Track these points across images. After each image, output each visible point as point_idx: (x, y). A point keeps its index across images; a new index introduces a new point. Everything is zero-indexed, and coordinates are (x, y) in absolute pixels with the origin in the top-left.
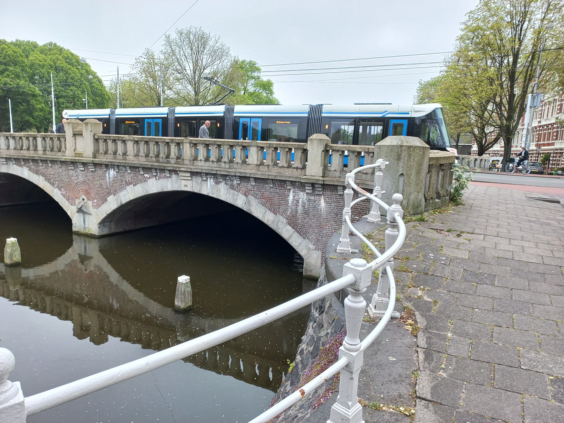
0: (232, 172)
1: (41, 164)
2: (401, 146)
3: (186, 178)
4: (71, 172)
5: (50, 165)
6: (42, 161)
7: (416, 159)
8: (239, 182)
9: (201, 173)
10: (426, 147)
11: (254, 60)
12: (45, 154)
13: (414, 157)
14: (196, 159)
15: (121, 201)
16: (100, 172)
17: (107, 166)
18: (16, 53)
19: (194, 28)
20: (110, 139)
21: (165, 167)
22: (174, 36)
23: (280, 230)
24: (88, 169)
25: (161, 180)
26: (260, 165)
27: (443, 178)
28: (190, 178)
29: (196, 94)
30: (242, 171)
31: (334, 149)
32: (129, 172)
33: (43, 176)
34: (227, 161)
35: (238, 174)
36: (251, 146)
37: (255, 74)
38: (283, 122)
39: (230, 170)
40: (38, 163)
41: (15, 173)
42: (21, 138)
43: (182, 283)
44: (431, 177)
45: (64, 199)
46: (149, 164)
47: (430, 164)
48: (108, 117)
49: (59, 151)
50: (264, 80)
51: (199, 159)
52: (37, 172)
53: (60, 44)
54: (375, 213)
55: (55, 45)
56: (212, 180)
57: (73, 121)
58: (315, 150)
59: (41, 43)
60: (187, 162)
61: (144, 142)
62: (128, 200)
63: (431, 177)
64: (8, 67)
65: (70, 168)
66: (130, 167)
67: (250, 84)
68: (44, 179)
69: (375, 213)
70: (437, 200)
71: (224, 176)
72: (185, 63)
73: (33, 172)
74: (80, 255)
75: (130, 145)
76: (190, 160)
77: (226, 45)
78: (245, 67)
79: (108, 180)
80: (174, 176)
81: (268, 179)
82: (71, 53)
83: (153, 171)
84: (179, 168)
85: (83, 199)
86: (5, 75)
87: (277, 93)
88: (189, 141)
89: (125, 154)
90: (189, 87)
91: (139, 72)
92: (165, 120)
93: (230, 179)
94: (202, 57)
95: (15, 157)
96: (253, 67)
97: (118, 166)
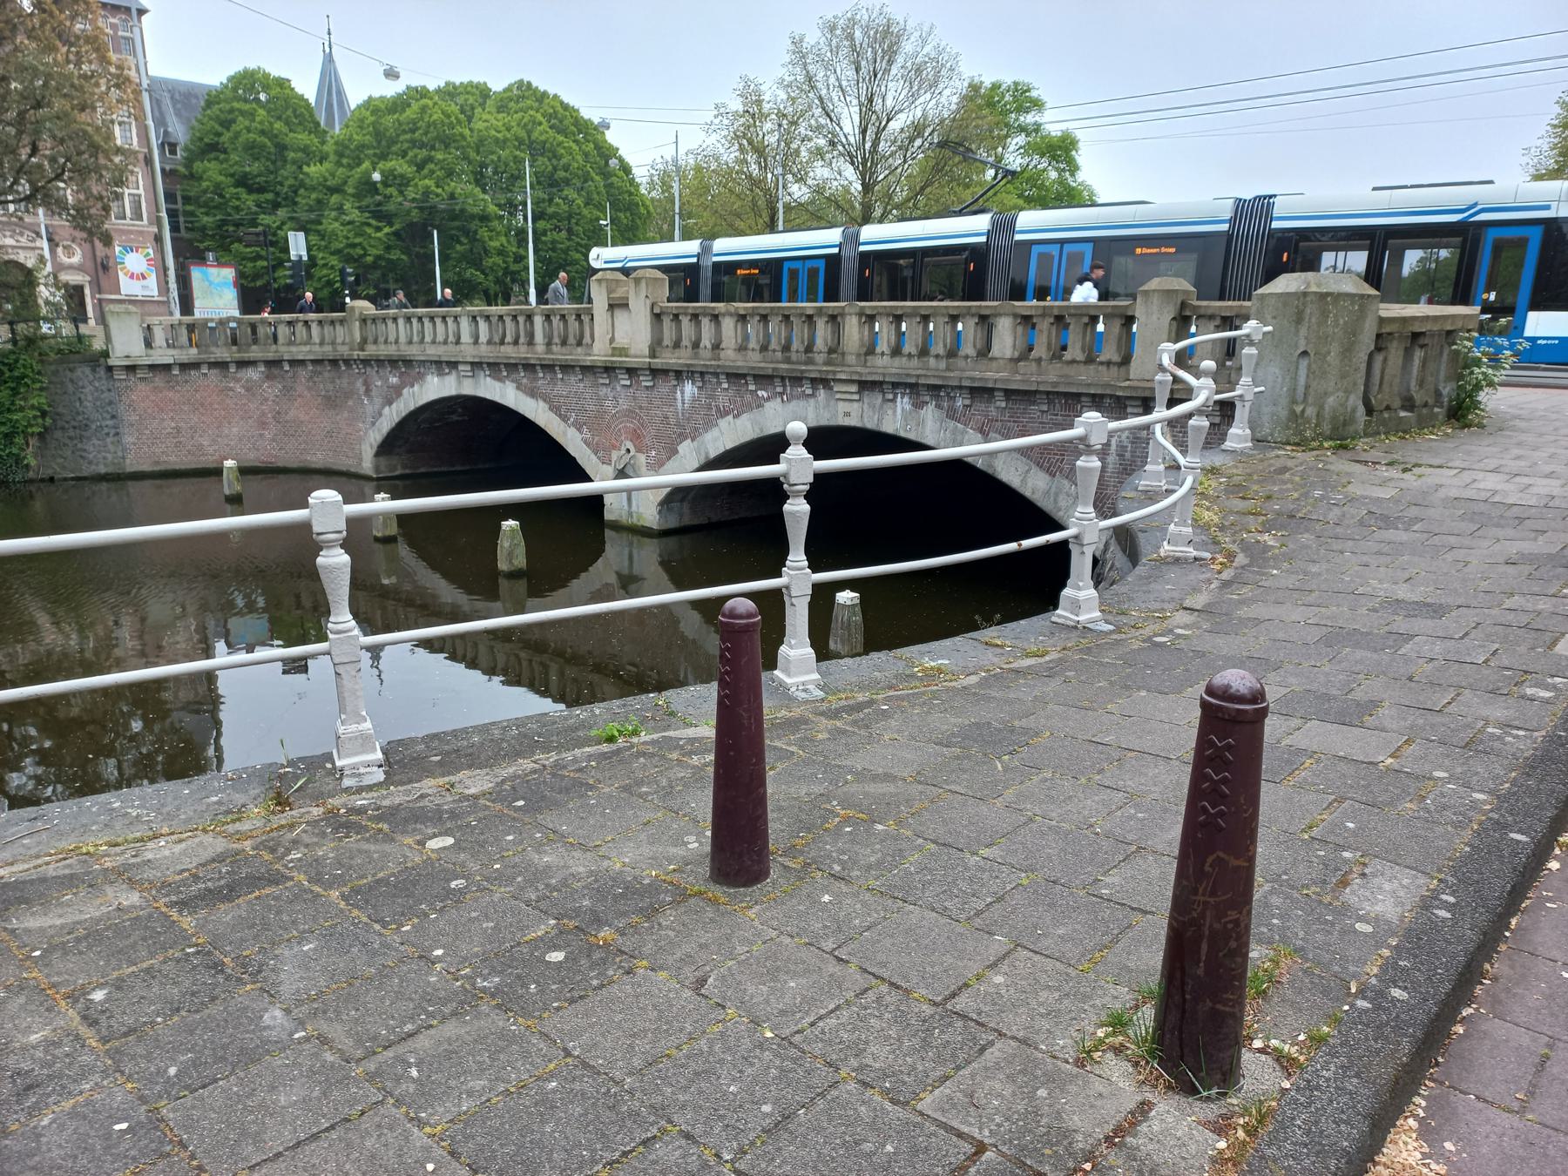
0: (953, 378)
1: (541, 375)
2: (1305, 294)
3: (848, 396)
4: (604, 391)
5: (560, 376)
6: (543, 366)
7: (1341, 322)
8: (967, 402)
9: (881, 383)
10: (1369, 296)
11: (1024, 78)
12: (549, 351)
13: (1336, 316)
14: (871, 351)
15: (707, 453)
16: (664, 387)
17: (678, 374)
18: (448, 116)
19: (864, 11)
20: (686, 314)
21: (802, 371)
22: (814, 37)
23: (1061, 513)
24: (639, 383)
25: (794, 403)
26: (1019, 360)
27: (1423, 366)
28: (856, 397)
29: (867, 188)
30: (977, 374)
31: (1202, 312)
32: (725, 386)
33: (545, 401)
34: (941, 351)
35: (966, 383)
36: (1000, 315)
37: (1029, 119)
38: (1155, 251)
39: (948, 374)
40: (535, 372)
41: (488, 397)
42: (501, 317)
43: (844, 606)
44: (1385, 360)
45: (589, 451)
46: (768, 367)
47: (1384, 331)
48: (694, 260)
49: (579, 344)
50: (1053, 134)
51: (878, 350)
52: (533, 393)
53: (541, 84)
54: (1240, 432)
55: (529, 84)
56: (906, 399)
57: (609, 275)
58: (1155, 317)
59: (497, 85)
60: (851, 359)
61: (758, 318)
62: (722, 450)
63: (1385, 360)
64: (433, 153)
65: (601, 381)
66: (728, 375)
67: (1011, 148)
68: (547, 406)
69: (1240, 432)
70: (1403, 414)
71: (935, 389)
72: (839, 109)
73: (524, 392)
74: (619, 575)
75: (728, 324)
76: (858, 355)
77: (948, 50)
78: (999, 102)
79: (679, 404)
80: (822, 393)
81: (1036, 392)
82: (562, 103)
83: (777, 381)
84: (834, 373)
85: (628, 451)
86: (426, 171)
87: (1092, 171)
88: (857, 310)
89: (716, 346)
90: (850, 173)
91: (723, 141)
92: (833, 262)
93: (948, 395)
94: (883, 89)
95: (491, 361)
96: (1024, 100)
97: (702, 374)
